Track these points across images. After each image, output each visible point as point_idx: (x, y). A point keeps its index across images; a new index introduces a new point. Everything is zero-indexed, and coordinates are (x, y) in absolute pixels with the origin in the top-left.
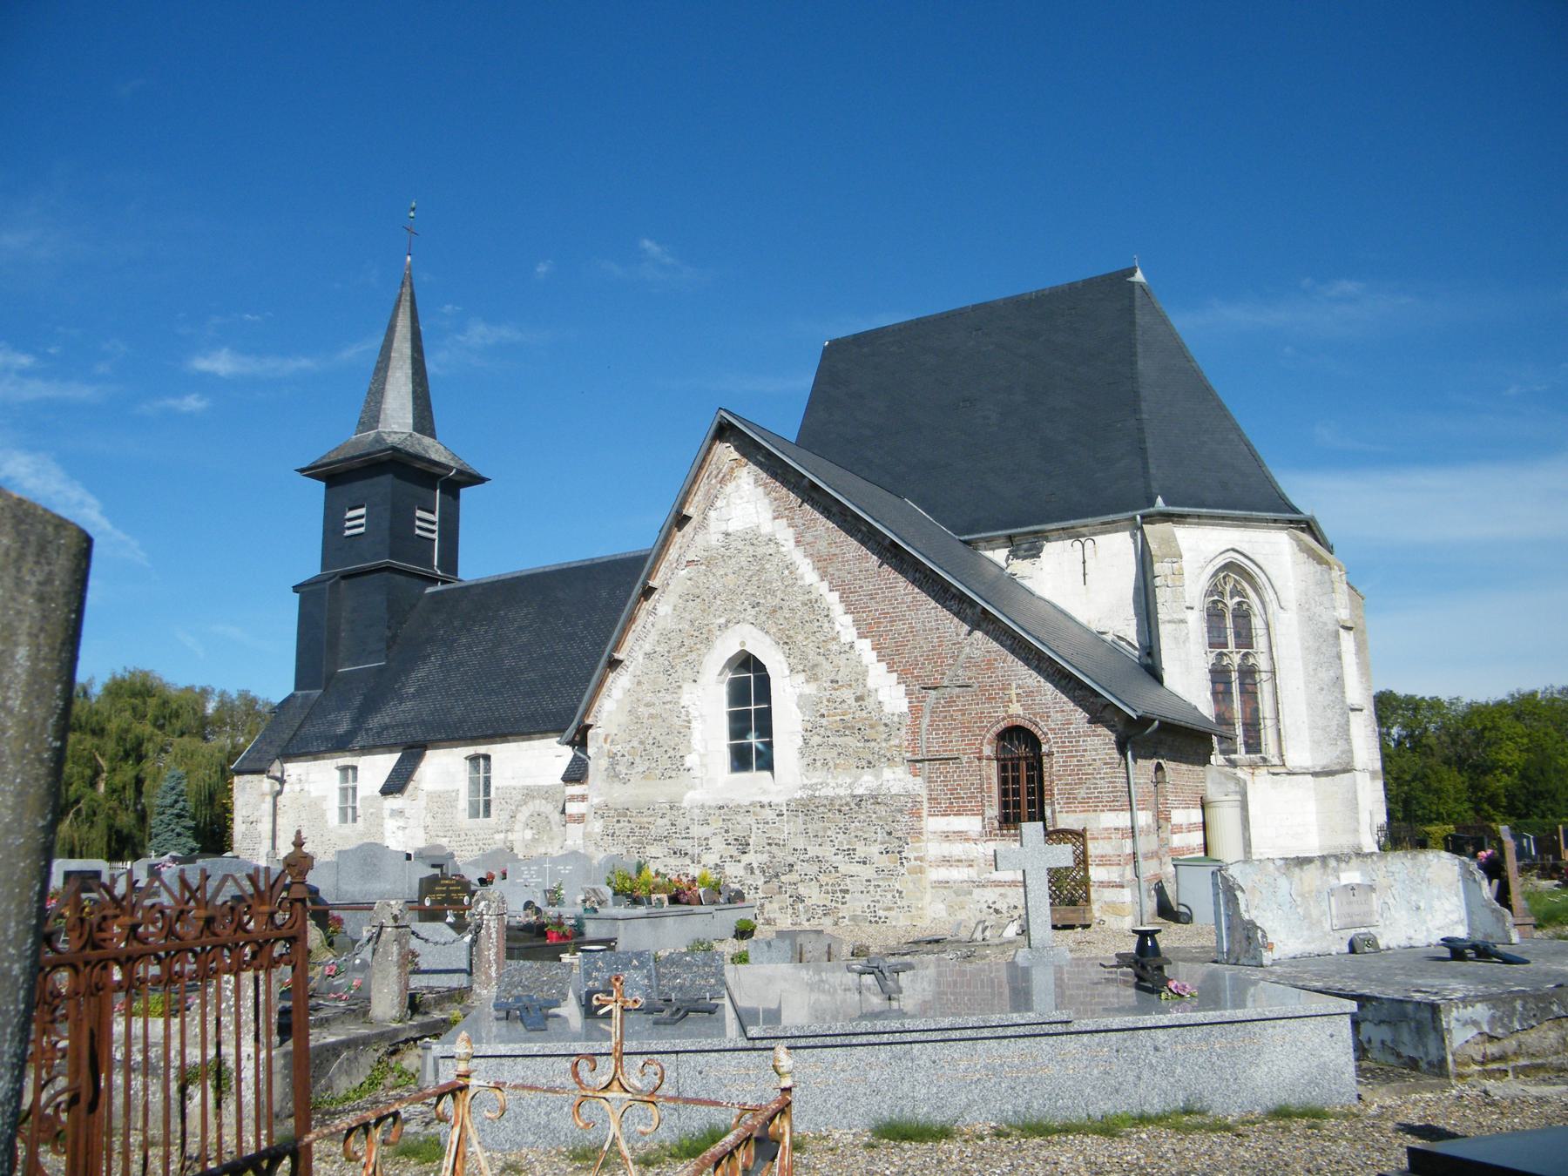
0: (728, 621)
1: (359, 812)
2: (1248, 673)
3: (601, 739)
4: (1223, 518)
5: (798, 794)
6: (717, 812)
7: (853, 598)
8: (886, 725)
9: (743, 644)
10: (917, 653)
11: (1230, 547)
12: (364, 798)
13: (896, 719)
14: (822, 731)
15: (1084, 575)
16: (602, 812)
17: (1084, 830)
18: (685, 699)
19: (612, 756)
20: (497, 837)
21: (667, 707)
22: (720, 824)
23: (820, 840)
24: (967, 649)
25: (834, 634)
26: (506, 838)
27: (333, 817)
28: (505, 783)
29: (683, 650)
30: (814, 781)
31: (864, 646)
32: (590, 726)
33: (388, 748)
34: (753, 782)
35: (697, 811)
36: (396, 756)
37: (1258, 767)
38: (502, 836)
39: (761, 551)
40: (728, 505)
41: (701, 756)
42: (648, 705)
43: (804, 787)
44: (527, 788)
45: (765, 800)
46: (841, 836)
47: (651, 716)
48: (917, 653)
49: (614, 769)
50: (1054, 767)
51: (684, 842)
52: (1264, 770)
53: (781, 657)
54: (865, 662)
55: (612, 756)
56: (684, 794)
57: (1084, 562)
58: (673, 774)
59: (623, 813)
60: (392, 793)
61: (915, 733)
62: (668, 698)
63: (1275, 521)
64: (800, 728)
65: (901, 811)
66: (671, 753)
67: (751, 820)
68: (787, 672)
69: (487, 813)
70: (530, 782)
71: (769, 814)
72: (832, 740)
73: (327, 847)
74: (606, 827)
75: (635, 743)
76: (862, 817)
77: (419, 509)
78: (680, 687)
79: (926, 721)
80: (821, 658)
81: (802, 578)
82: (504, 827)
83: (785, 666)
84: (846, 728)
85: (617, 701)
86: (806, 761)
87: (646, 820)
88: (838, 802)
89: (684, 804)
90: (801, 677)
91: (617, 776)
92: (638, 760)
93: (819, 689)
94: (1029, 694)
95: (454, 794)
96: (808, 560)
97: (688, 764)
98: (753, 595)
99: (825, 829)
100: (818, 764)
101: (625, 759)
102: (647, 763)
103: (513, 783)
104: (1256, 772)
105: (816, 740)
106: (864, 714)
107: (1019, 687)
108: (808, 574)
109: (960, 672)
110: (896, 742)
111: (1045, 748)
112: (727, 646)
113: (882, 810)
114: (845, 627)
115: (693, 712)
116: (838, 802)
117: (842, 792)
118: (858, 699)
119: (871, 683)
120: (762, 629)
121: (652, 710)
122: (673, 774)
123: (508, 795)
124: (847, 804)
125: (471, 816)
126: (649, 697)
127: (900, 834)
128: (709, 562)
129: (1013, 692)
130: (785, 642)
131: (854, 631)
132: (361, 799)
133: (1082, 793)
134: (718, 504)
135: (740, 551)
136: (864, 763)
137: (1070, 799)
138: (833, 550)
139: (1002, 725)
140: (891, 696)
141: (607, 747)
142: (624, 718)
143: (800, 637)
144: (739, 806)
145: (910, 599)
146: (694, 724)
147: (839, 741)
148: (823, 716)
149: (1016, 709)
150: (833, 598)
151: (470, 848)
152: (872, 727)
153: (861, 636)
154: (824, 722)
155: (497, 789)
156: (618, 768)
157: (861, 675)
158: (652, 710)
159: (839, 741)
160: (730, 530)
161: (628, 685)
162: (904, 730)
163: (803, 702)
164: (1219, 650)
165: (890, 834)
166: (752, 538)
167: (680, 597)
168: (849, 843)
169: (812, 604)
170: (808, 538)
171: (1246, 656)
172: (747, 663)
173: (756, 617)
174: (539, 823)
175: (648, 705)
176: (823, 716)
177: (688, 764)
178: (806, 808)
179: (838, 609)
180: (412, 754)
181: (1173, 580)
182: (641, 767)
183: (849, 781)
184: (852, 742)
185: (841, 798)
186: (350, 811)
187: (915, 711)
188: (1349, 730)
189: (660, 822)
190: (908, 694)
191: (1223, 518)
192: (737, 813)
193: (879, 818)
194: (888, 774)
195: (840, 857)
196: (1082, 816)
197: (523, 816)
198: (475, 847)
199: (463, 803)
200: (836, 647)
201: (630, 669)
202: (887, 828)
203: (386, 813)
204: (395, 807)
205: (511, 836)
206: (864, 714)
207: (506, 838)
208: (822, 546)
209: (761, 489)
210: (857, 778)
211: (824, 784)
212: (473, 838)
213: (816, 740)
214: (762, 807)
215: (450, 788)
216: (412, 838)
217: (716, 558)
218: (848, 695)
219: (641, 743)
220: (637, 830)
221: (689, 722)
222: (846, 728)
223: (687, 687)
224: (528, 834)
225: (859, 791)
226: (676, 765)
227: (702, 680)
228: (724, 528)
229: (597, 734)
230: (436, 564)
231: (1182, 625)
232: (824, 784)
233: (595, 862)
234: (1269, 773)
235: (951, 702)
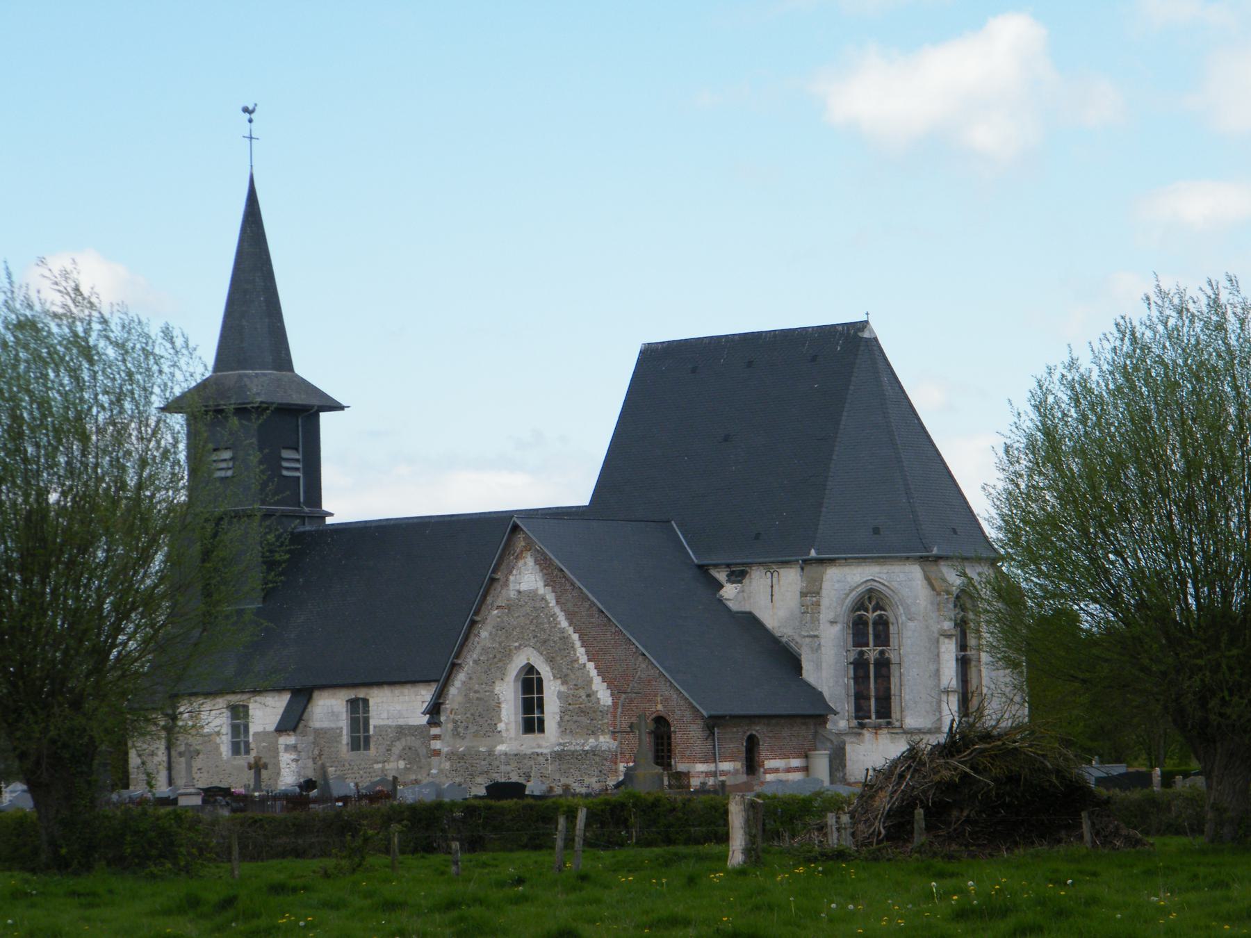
0: (520, 645)
1: (252, 746)
2: (884, 665)
3: (449, 711)
4: (865, 558)
5: (557, 748)
6: (514, 758)
7: (586, 637)
8: (601, 711)
9: (528, 659)
10: (616, 672)
11: (870, 578)
12: (255, 734)
13: (606, 708)
14: (569, 713)
15: (772, 595)
16: (451, 756)
17: (689, 772)
18: (497, 689)
19: (455, 722)
20: (376, 766)
21: (487, 694)
22: (516, 764)
23: (567, 775)
24: (639, 673)
25: (575, 658)
26: (384, 767)
27: (225, 749)
28: (382, 723)
29: (496, 660)
30: (566, 741)
31: (591, 666)
32: (442, 704)
33: (279, 690)
34: (531, 743)
35: (503, 757)
36: (285, 698)
37: (880, 728)
38: (380, 766)
39: (538, 605)
40: (520, 574)
41: (507, 724)
42: (476, 692)
43: (560, 744)
44: (400, 727)
45: (539, 751)
46: (577, 773)
47: (478, 699)
48: (616, 672)
49: (456, 730)
50: (677, 738)
51: (495, 775)
52: (885, 731)
53: (548, 669)
54: (591, 675)
55: (455, 722)
56: (496, 746)
57: (772, 587)
58: (490, 734)
59: (462, 757)
60: (286, 731)
61: (615, 717)
62: (487, 689)
63: (908, 558)
64: (558, 711)
65: (606, 759)
66: (489, 722)
67: (532, 763)
68: (552, 678)
69: (367, 747)
70: (401, 722)
71: (541, 759)
72: (575, 718)
73: (222, 777)
74: (452, 766)
75: (468, 715)
76: (588, 762)
77: (285, 448)
78: (494, 682)
79: (619, 710)
80: (569, 671)
81: (560, 624)
82: (381, 759)
83: (551, 674)
84: (582, 712)
85: (458, 688)
86: (561, 730)
87: (475, 761)
88: (576, 754)
89: (496, 753)
90: (559, 682)
91: (458, 734)
92: (470, 726)
93: (568, 689)
94: (666, 700)
95: (338, 731)
96: (563, 613)
97: (499, 729)
98: (534, 630)
99: (570, 768)
100: (568, 731)
101: (463, 724)
102: (476, 727)
103: (389, 722)
104: (879, 732)
105: (567, 718)
106: (590, 704)
107: (661, 696)
108: (564, 623)
109: (636, 685)
110: (606, 721)
111: (672, 729)
112: (519, 661)
113: (597, 759)
114: (581, 652)
115: (502, 699)
116: (576, 754)
117: (578, 748)
118: (588, 696)
119: (594, 688)
120: (539, 652)
121: (477, 695)
122: (490, 734)
123: (384, 733)
124: (580, 755)
125: (353, 749)
126: (477, 687)
127: (605, 772)
128: (509, 607)
129: (659, 699)
130: (550, 660)
131: (585, 657)
132: (253, 735)
133: (688, 753)
134: (514, 572)
135: (526, 603)
136: (590, 732)
137: (683, 756)
138: (577, 610)
139: (654, 715)
140: (604, 696)
141: (452, 716)
142: (460, 699)
143: (559, 658)
144: (525, 754)
145: (613, 642)
146: (503, 705)
147: (579, 719)
148: (570, 704)
149: (660, 707)
150: (575, 637)
151: (353, 776)
152: (594, 712)
153: (589, 660)
154: (570, 707)
155: (375, 727)
156: (459, 730)
157: (590, 681)
158: (477, 695)
159: (579, 719)
160: (522, 589)
161: (464, 679)
162: (609, 715)
163: (560, 696)
164: (859, 649)
165: (601, 771)
166: (532, 595)
167: (494, 627)
168: (581, 776)
169: (565, 639)
170: (563, 600)
171: (882, 653)
172: (530, 669)
173: (535, 644)
174: (410, 755)
175: (476, 692)
176: (570, 704)
177: (499, 729)
178: (559, 756)
179: (578, 644)
180: (302, 696)
181: (812, 609)
182: (473, 729)
183: (582, 741)
184: (585, 720)
185: (577, 751)
186: (242, 745)
187: (615, 704)
188: (657, 744)
189: (483, 763)
190: (612, 695)
191: (865, 558)
192: (525, 758)
193: (596, 763)
194: (602, 739)
195: (576, 784)
196: (688, 765)
197: (398, 747)
198: (357, 775)
199: (345, 739)
200: (577, 666)
201: (466, 669)
202: (600, 769)
203: (281, 748)
204: (288, 743)
205: (387, 766)
206: (590, 704)
207: (384, 767)
208: (570, 605)
209: (537, 566)
210: (587, 740)
211: (571, 743)
212: (356, 768)
213: (567, 718)
214: (538, 755)
215: (333, 725)
216: (304, 768)
217: (513, 606)
218: (582, 693)
219: (472, 715)
220: (469, 767)
221: (499, 703)
222: (582, 712)
223: (497, 683)
224: (402, 764)
225: (587, 748)
226: (492, 730)
227: (506, 679)
228: (517, 588)
229: (446, 708)
230: (302, 500)
231: (816, 639)
232: (571, 743)
233: (695, 782)
234: (888, 733)
235: (631, 701)
